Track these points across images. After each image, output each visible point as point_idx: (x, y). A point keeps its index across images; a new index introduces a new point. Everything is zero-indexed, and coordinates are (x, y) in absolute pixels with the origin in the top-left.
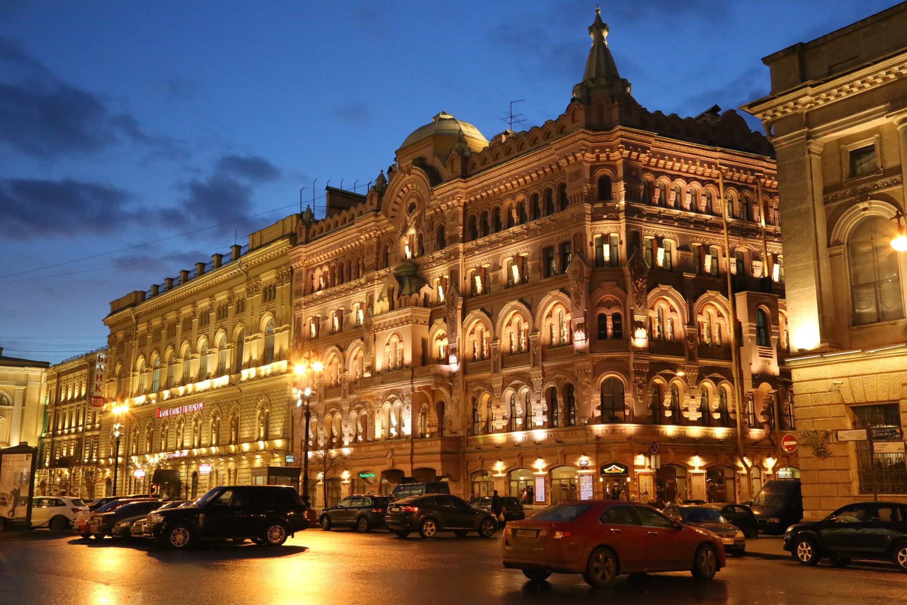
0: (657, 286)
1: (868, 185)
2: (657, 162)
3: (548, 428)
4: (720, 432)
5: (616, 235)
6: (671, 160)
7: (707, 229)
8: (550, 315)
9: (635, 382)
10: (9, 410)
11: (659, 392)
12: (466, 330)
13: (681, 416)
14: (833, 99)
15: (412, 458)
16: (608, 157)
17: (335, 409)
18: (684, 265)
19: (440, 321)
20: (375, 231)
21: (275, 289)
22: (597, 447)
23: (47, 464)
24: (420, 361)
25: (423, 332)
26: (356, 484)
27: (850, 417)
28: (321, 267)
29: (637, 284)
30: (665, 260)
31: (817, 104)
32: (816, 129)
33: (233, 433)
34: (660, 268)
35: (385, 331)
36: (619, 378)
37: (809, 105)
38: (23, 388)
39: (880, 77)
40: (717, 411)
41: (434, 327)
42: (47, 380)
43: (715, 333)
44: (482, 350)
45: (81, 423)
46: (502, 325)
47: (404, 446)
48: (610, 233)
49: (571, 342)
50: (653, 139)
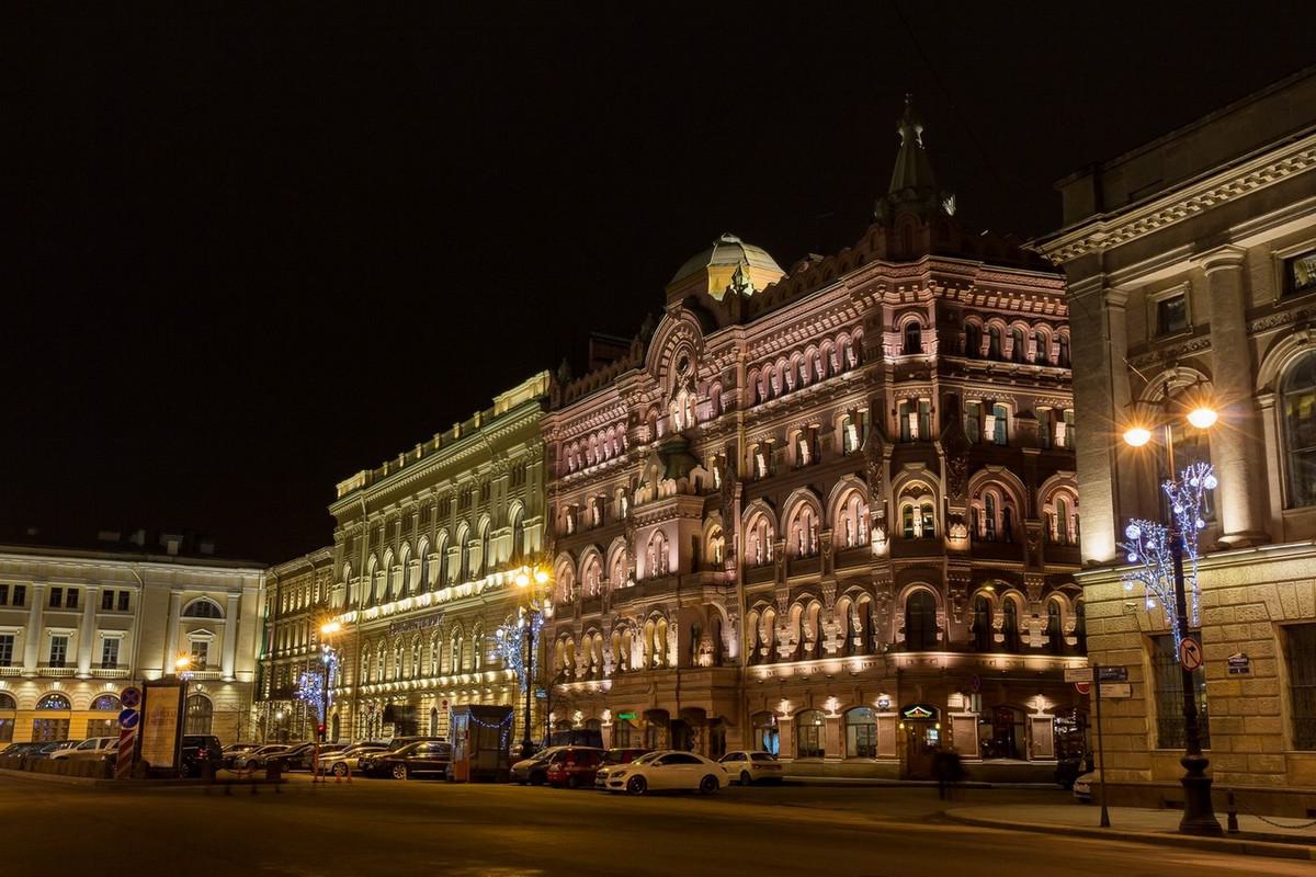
1: (1176, 347)
2: (986, 300)
3: (862, 655)
6: (1005, 295)
7: (1060, 387)
8: (844, 508)
9: (950, 596)
11: (986, 607)
12: (746, 525)
13: (1019, 640)
15: (678, 695)
16: (916, 296)
17: (765, 602)
18: (1024, 438)
19: (715, 513)
21: (525, 469)
22: (899, 683)
23: (267, 695)
24: (690, 566)
26: (620, 727)
27: (1148, 649)
29: (953, 466)
32: (1231, 229)
34: (990, 442)
37: (1104, 244)
38: (237, 596)
40: (1072, 634)
41: (709, 521)
42: (267, 585)
44: (810, 543)
45: (304, 642)
46: (834, 510)
47: (669, 678)
48: (918, 398)
49: (869, 544)
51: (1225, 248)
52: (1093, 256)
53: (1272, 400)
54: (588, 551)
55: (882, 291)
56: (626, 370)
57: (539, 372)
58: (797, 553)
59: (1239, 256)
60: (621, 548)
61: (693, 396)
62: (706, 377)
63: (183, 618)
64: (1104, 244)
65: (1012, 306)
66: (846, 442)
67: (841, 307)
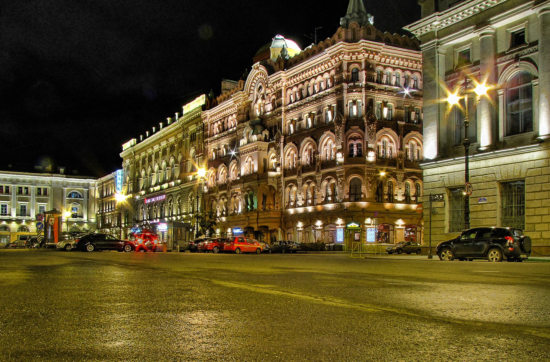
0: (382, 128)
4: (414, 207)
5: (361, 101)
10: (82, 200)
12: (285, 153)
14: (455, 21)
15: (257, 221)
18: (398, 118)
20: (242, 102)
21: (196, 135)
25: (264, 155)
27: (448, 194)
28: (217, 122)
29: (370, 128)
30: (388, 114)
31: (442, 26)
33: (179, 210)
35: (245, 155)
36: (356, 176)
37: (438, 27)
39: (471, 11)
40: (414, 196)
41: (270, 152)
42: (98, 186)
43: (416, 154)
46: (302, 150)
50: (382, 47)
51: (488, 27)
52: (433, 33)
53: (503, 92)
54: (221, 166)
55: (343, 55)
56: (236, 92)
57: (201, 95)
58: (306, 164)
59: (493, 31)
60: (235, 165)
61: (264, 101)
62: (269, 93)
63: (67, 198)
64: (438, 27)
65: (391, 63)
66: (327, 118)
67: (325, 62)
